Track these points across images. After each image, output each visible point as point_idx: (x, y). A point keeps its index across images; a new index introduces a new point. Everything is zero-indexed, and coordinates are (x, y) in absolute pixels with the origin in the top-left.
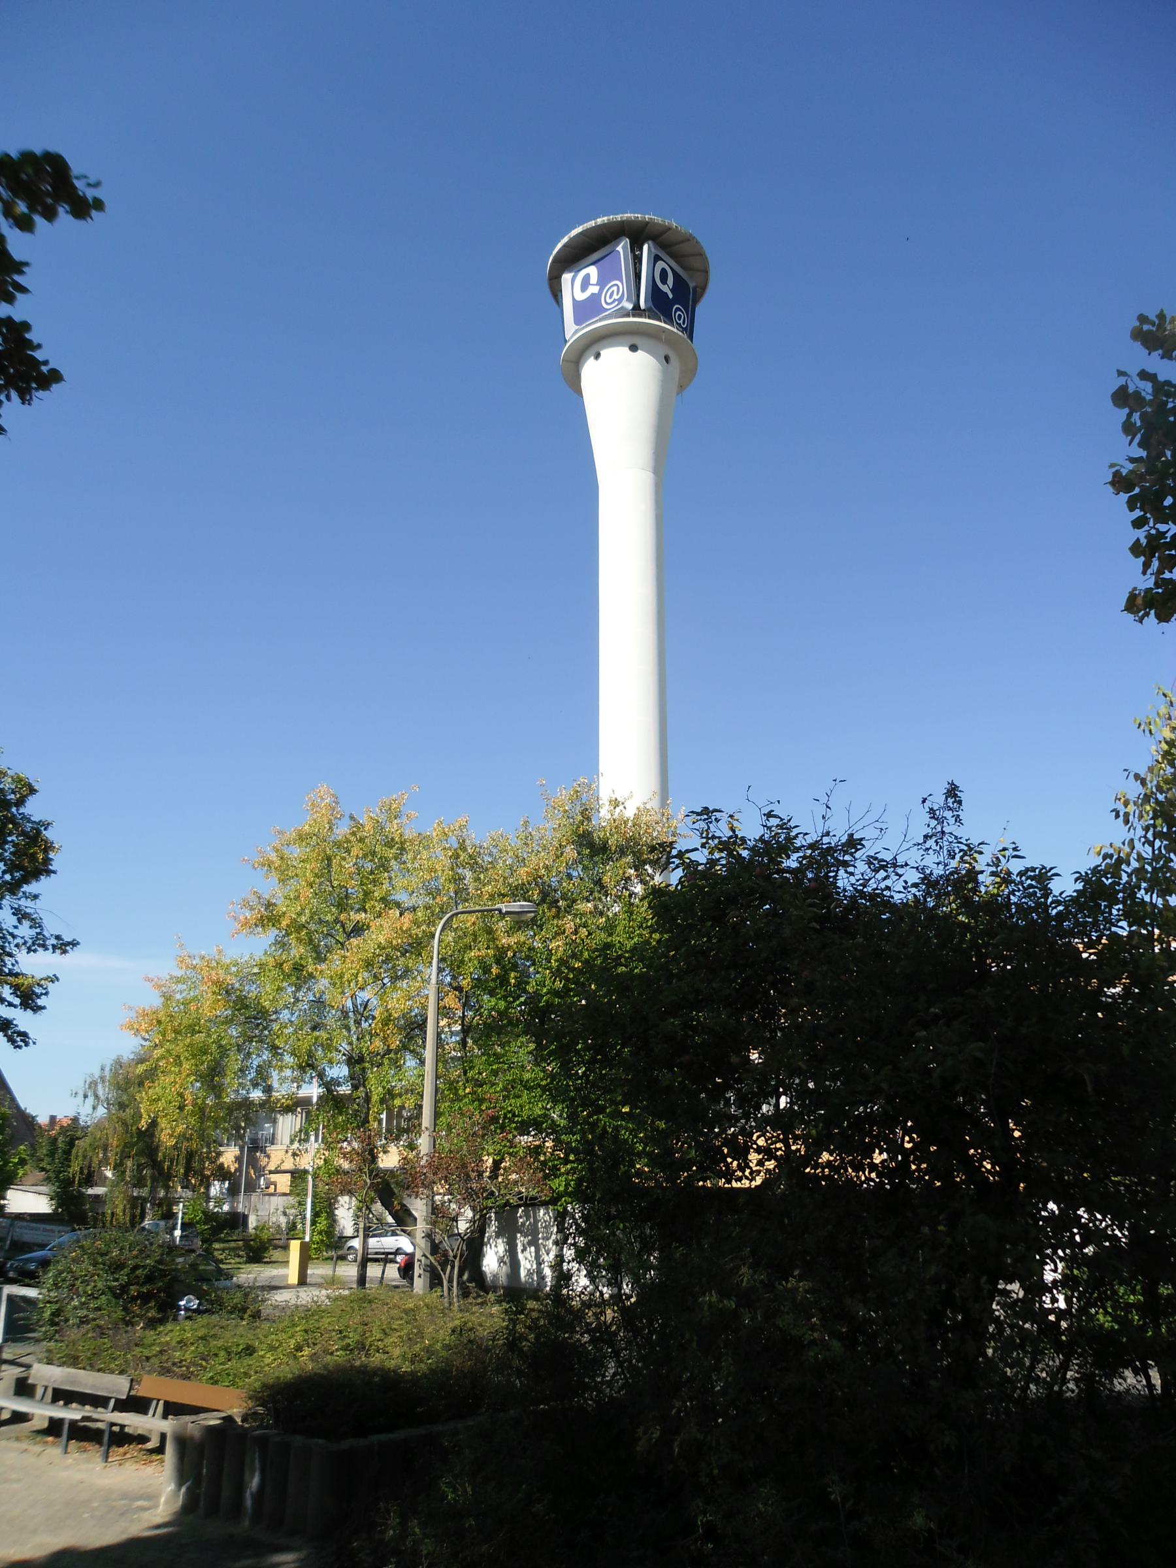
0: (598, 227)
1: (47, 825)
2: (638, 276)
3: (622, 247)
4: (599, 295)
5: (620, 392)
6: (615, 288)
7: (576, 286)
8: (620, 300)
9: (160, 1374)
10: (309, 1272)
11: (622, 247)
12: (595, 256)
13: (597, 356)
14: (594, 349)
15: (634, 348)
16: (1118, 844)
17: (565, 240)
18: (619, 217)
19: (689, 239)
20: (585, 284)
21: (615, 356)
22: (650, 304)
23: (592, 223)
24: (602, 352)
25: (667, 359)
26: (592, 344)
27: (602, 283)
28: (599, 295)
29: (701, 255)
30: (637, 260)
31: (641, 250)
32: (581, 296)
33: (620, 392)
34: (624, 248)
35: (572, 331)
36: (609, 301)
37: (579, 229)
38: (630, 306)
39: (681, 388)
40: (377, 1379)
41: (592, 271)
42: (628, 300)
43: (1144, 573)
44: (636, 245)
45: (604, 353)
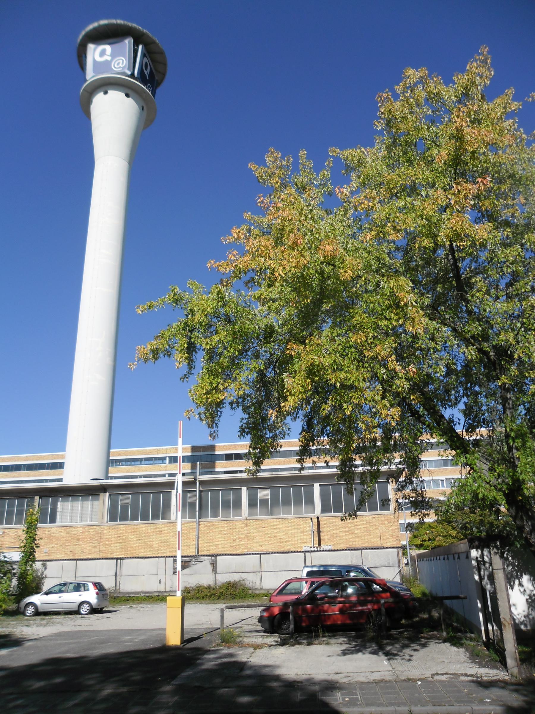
0: (117, 25)
3: (128, 42)
5: (113, 119)
6: (121, 61)
7: (96, 53)
8: (123, 68)
10: (111, 450)
11: (128, 42)
12: (111, 41)
13: (106, 93)
14: (105, 88)
15: (127, 95)
16: (223, 410)
17: (96, 24)
18: (130, 24)
19: (162, 53)
20: (103, 53)
22: (139, 76)
24: (109, 91)
25: (143, 108)
26: (105, 85)
29: (165, 64)
30: (135, 52)
31: (138, 47)
32: (98, 59)
33: (113, 119)
34: (129, 43)
35: (91, 75)
36: (116, 66)
38: (129, 73)
39: (144, 128)
40: (275, 684)
41: (108, 48)
44: (136, 43)
45: (110, 92)
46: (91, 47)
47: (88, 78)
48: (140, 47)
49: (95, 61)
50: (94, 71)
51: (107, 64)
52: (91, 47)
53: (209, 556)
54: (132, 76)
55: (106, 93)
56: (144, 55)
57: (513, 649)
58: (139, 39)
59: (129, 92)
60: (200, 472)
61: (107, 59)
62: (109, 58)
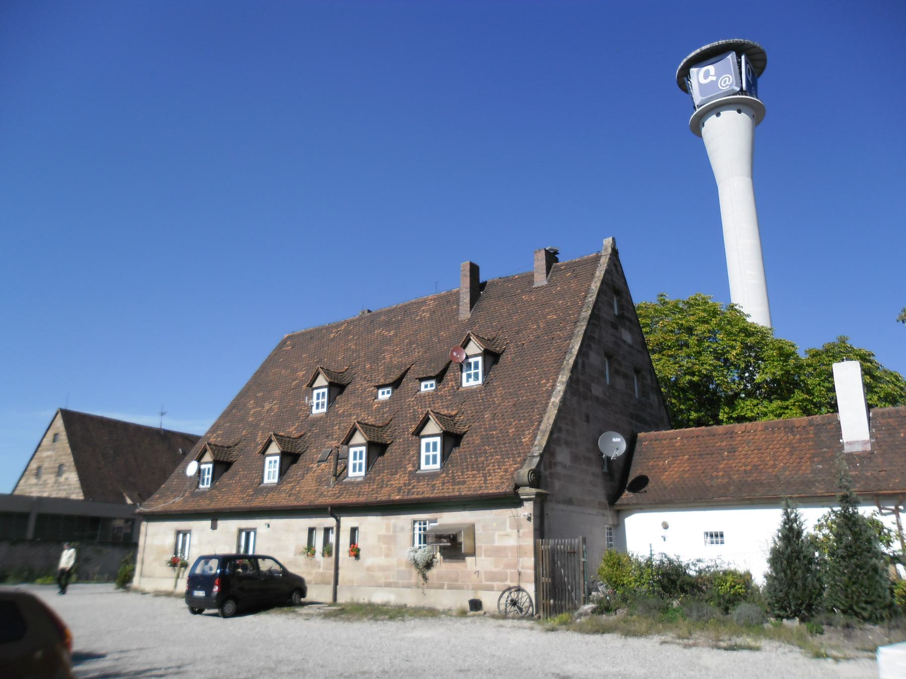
1: (214, 527)
2: (741, 73)
4: (717, 81)
5: (727, 139)
7: (700, 77)
8: (731, 85)
9: (837, 411)
11: (731, 57)
13: (718, 115)
14: (717, 111)
15: (739, 111)
19: (762, 53)
20: (707, 75)
21: (729, 115)
23: (716, 43)
26: (716, 109)
27: (718, 75)
28: (717, 81)
32: (703, 81)
33: (727, 139)
37: (708, 46)
38: (738, 89)
41: (711, 68)
42: (737, 85)
43: (758, 649)
46: (693, 71)
47: (697, 103)
48: (743, 57)
49: (700, 84)
50: (702, 94)
51: (713, 84)
52: (693, 71)
53: (31, 460)
54: (742, 91)
55: (718, 115)
56: (746, 63)
57: (882, 631)
58: (739, 49)
59: (740, 107)
60: (457, 302)
61: (713, 80)
62: (714, 78)
